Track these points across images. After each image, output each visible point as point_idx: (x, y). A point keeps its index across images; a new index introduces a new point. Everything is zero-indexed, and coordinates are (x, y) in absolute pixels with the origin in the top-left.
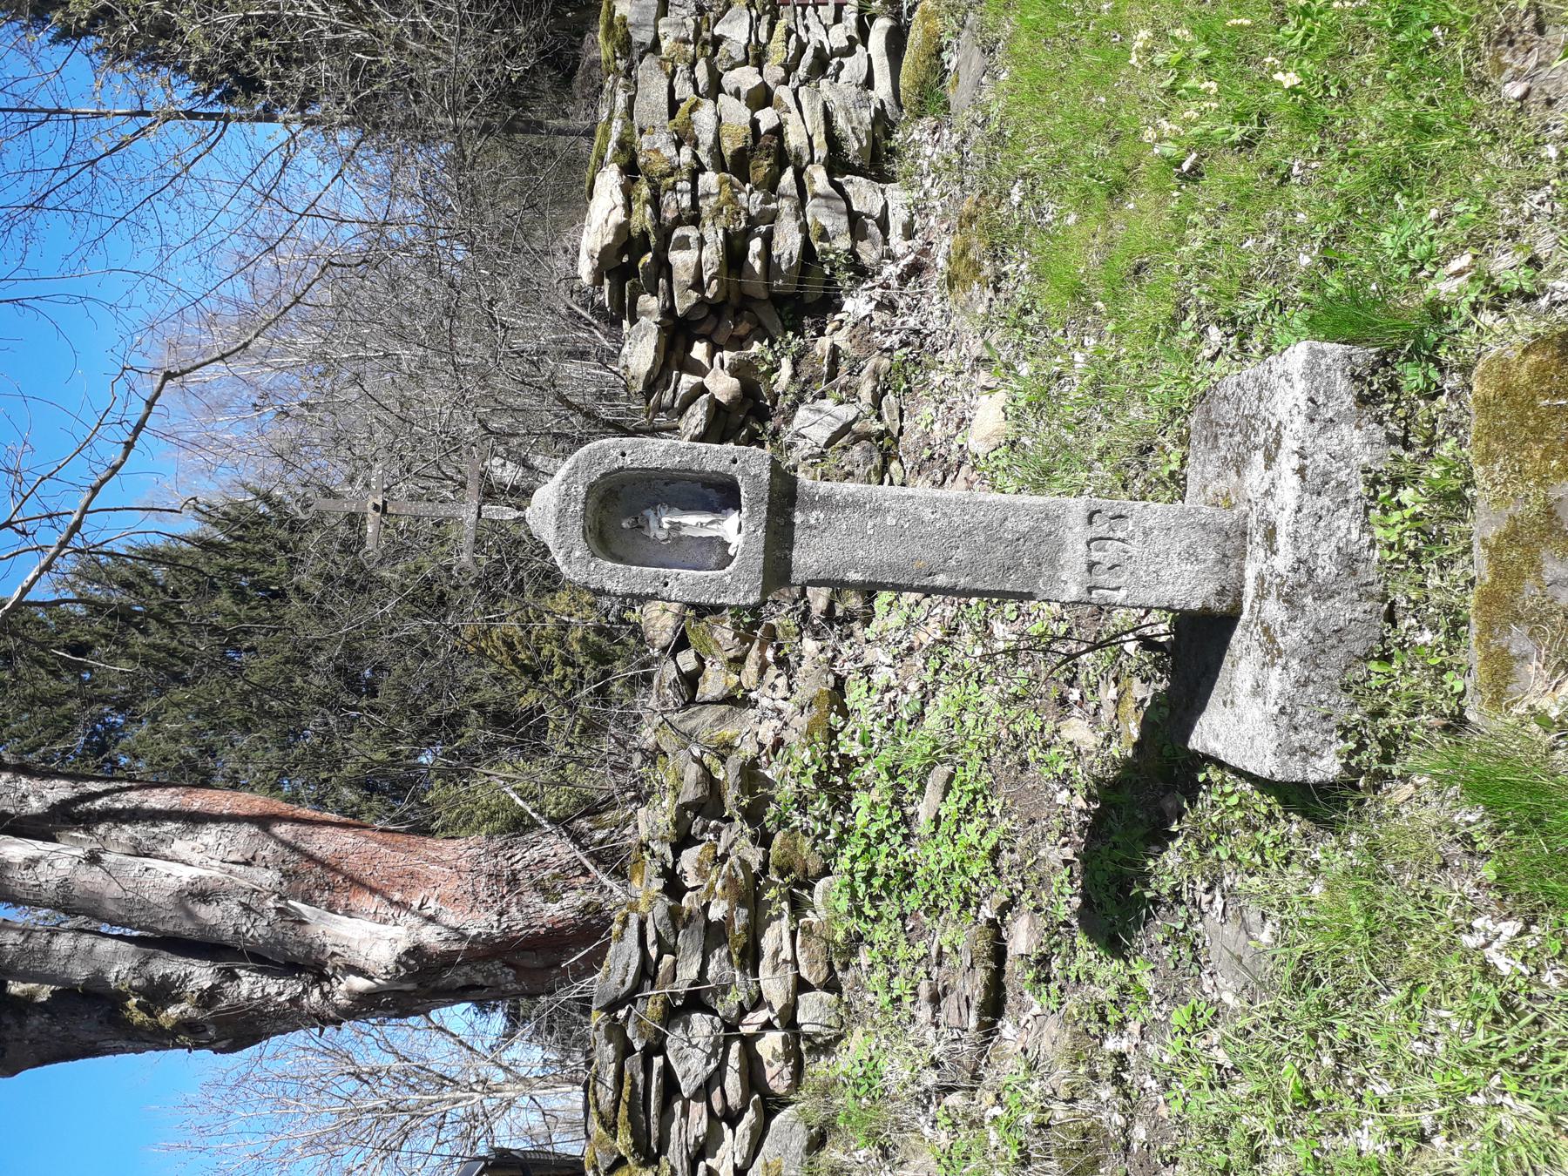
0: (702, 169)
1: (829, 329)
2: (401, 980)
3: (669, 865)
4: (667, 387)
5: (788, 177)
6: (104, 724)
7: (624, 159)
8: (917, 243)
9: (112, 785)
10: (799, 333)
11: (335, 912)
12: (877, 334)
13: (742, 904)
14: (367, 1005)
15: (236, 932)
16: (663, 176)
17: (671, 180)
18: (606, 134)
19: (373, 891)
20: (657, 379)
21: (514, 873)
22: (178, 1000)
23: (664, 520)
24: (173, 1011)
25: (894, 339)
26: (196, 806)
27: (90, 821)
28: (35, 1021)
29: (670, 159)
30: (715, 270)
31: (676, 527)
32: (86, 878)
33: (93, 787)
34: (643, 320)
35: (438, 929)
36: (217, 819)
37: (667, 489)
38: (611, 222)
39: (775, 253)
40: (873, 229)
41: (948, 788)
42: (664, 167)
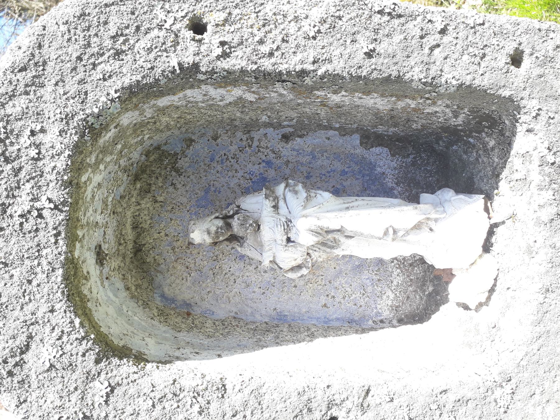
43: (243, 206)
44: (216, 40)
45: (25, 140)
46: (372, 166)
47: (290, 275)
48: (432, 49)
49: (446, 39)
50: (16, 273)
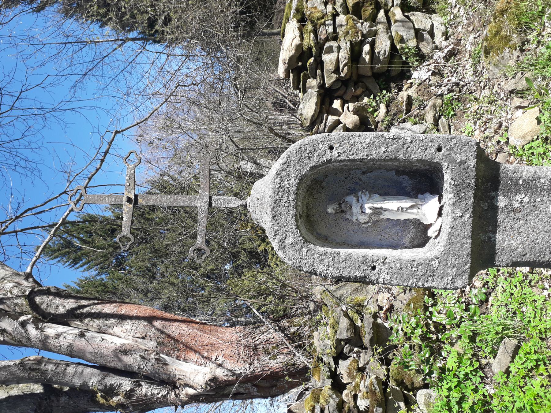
0: (337, 14)
1: (405, 87)
2: (208, 391)
3: (333, 369)
4: (321, 122)
5: (382, 13)
6: (121, 256)
7: (299, 17)
8: (452, 40)
9: (92, 302)
10: (389, 91)
11: (180, 360)
12: (433, 88)
13: (379, 406)
14: (194, 399)
15: (139, 368)
16: (319, 19)
17: (323, 21)
18: (290, 7)
19: (196, 351)
20: (316, 119)
21: (256, 346)
22: (117, 394)
23: (367, 206)
24: (115, 399)
25: (444, 89)
26: (123, 312)
27: (81, 317)
28: (63, 399)
29: (322, 11)
30: (346, 61)
31: (377, 211)
32: (79, 343)
33: (84, 302)
34: (310, 91)
35: (223, 370)
36: (131, 318)
37: (364, 178)
38: (293, 45)
39: (376, 51)
40: (427, 36)
41: (516, 352)
42: (319, 14)
43: (346, 200)
44: (337, 152)
45: (286, 182)
46: (401, 183)
47: (364, 225)
48: (407, 148)
49: (412, 145)
50: (283, 217)
